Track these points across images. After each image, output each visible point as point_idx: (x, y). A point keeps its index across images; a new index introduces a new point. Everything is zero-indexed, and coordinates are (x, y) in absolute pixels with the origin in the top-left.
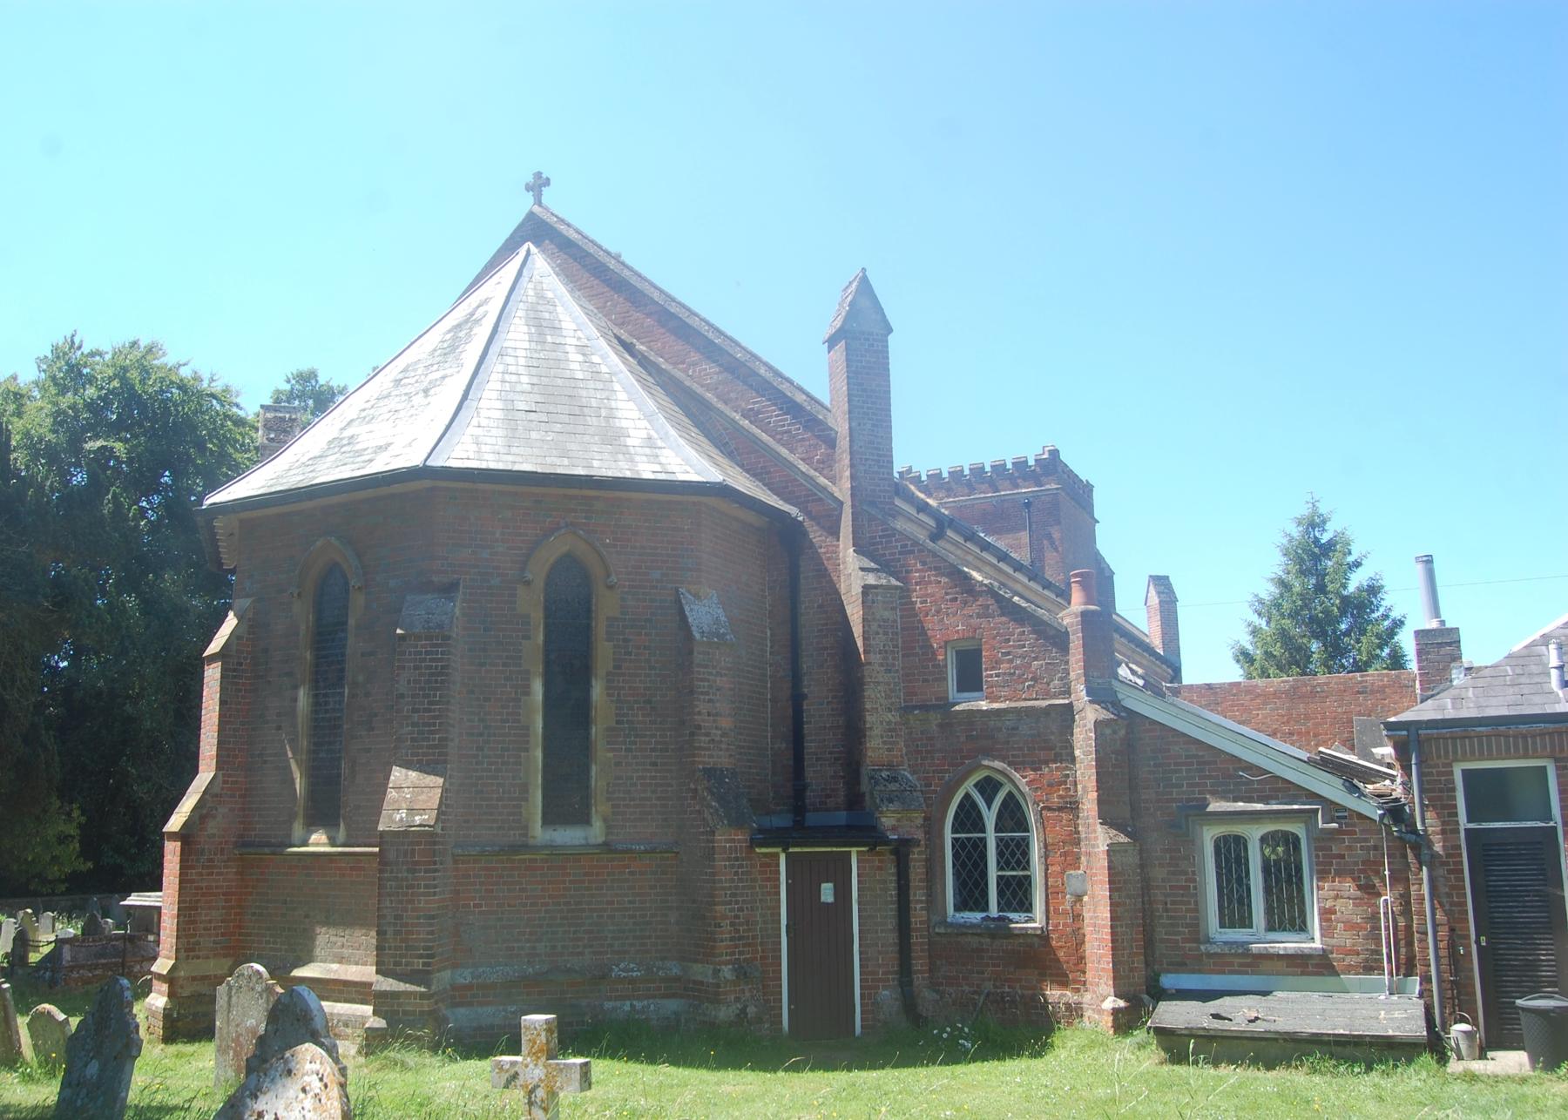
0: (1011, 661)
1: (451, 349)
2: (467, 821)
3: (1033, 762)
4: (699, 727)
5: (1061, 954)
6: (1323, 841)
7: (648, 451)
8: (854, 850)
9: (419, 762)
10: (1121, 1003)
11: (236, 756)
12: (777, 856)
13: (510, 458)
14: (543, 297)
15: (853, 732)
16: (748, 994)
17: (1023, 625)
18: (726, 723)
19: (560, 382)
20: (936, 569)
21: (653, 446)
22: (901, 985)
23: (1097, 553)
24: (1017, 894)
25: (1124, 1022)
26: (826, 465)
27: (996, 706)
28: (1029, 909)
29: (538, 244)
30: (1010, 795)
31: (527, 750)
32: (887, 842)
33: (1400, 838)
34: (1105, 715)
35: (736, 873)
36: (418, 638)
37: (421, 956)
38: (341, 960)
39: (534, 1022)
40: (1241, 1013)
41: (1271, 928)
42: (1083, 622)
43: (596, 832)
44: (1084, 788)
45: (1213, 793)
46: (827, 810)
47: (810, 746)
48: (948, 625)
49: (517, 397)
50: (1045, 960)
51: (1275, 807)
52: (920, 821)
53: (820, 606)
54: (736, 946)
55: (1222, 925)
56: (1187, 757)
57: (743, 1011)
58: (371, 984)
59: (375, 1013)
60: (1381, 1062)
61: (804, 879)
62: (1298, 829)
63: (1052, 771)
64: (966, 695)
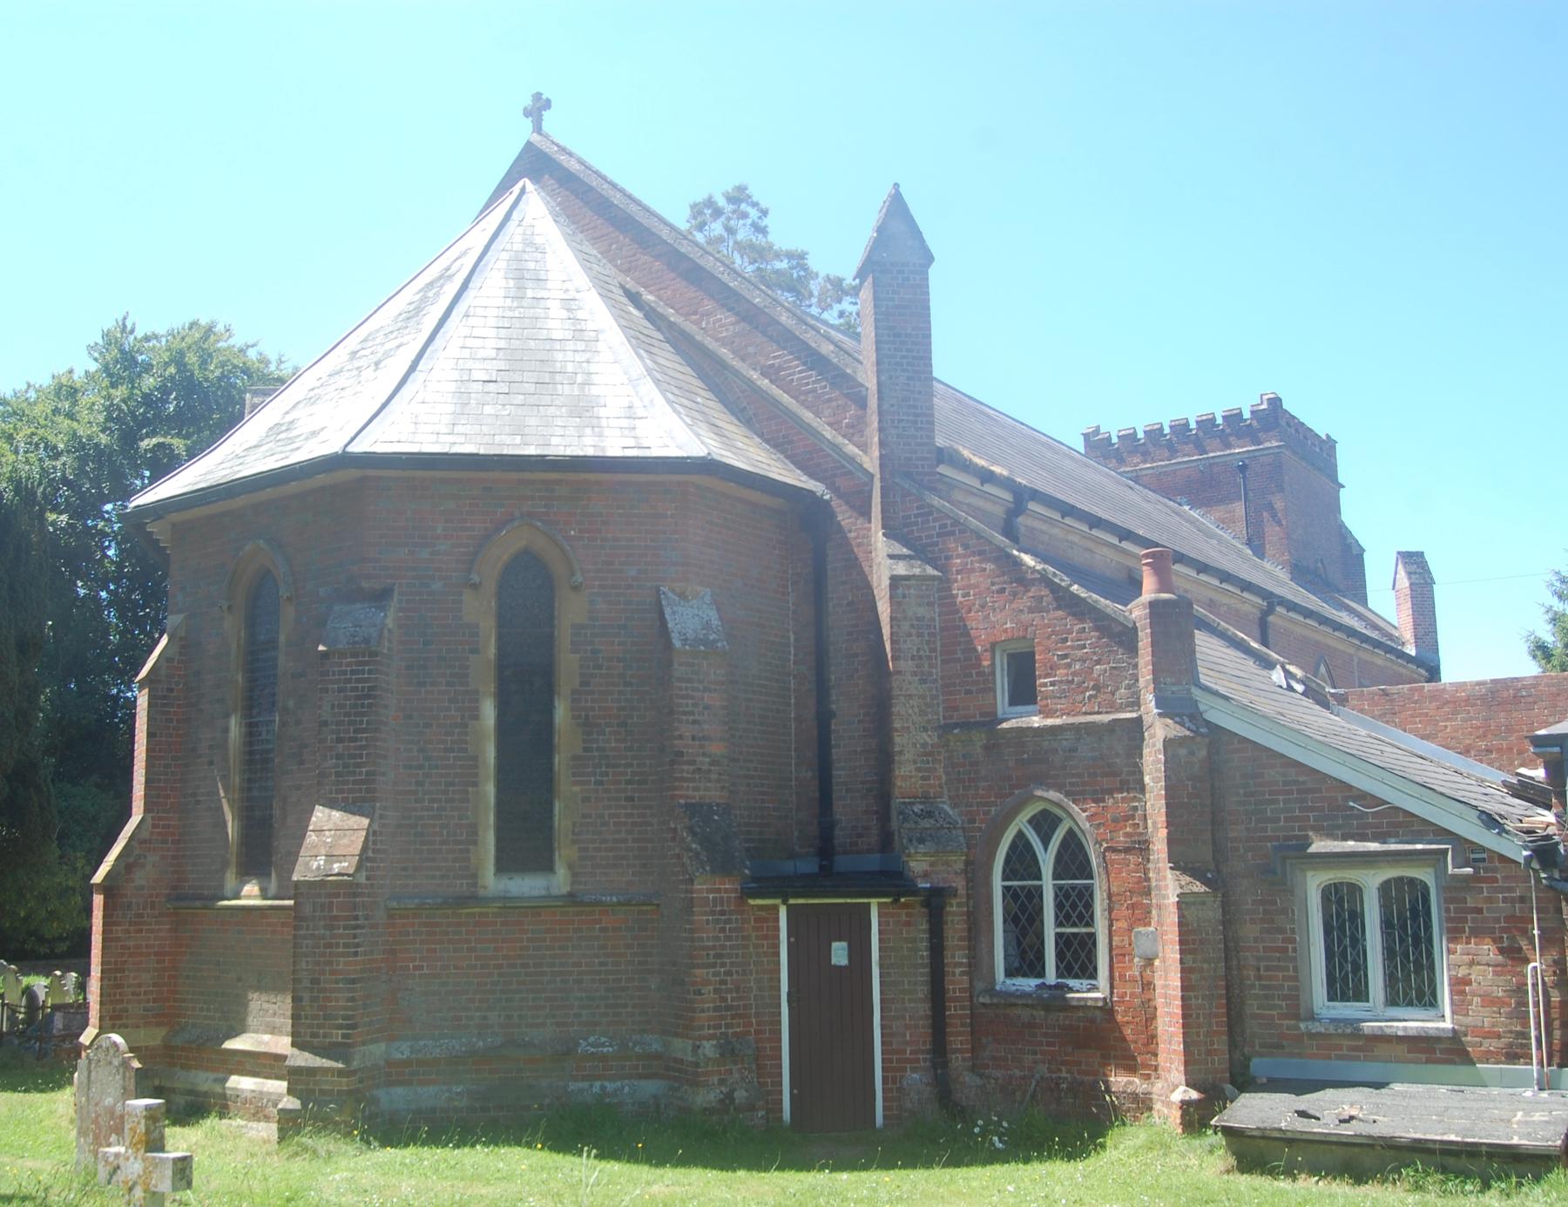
0: (1069, 666)
1: (416, 311)
2: (405, 869)
3: (1095, 792)
4: (680, 754)
5: (1128, 1031)
6: (1455, 889)
7: (625, 423)
8: (874, 902)
10: (1194, 1095)
11: (168, 797)
12: (775, 908)
13: (452, 438)
14: (532, 244)
15: (884, 758)
16: (736, 1076)
17: (1082, 621)
18: (717, 749)
19: (532, 344)
20: (981, 553)
21: (637, 412)
22: (935, 1066)
23: (1342, 526)
24: (1078, 957)
25: (1195, 1119)
26: (855, 430)
27: (1050, 722)
28: (1093, 975)
29: (536, 180)
30: (1070, 832)
31: (475, 784)
32: (913, 891)
33: (1550, 887)
34: (1177, 731)
35: (723, 930)
36: (342, 655)
37: (340, 1027)
39: (135, 1108)
40: (1340, 1110)
41: (1392, 1001)
42: (1152, 615)
43: (560, 882)
44: (1154, 823)
45: (1314, 828)
46: (858, 852)
47: (839, 774)
48: (994, 621)
49: (478, 365)
50: (1106, 1039)
51: (1393, 847)
52: (960, 866)
53: (850, 604)
54: (722, 1018)
55: (1332, 997)
56: (1285, 783)
57: (730, 1096)
58: (284, 1057)
59: (290, 1091)
60: (1500, 1179)
61: (810, 937)
62: (1425, 875)
63: (1117, 802)
64: (1020, 709)
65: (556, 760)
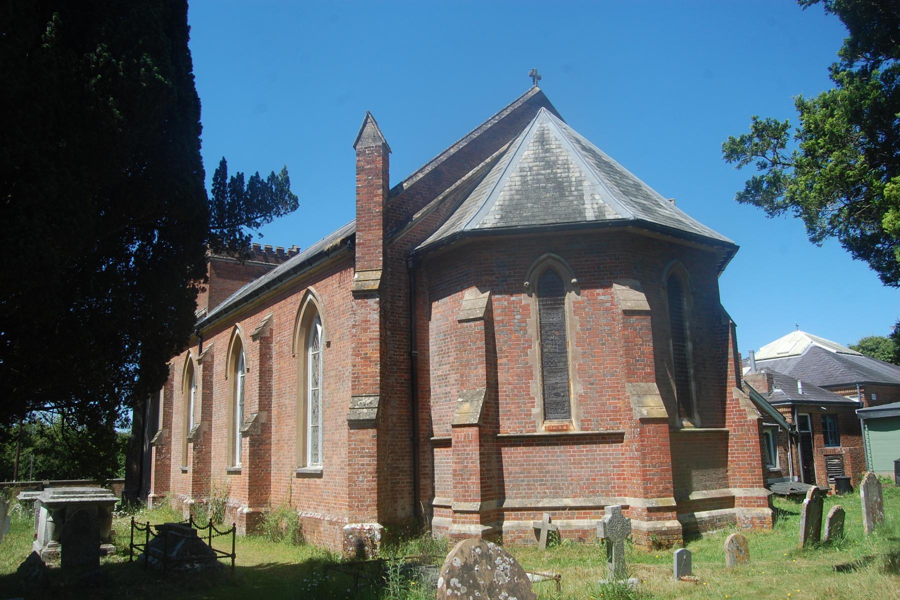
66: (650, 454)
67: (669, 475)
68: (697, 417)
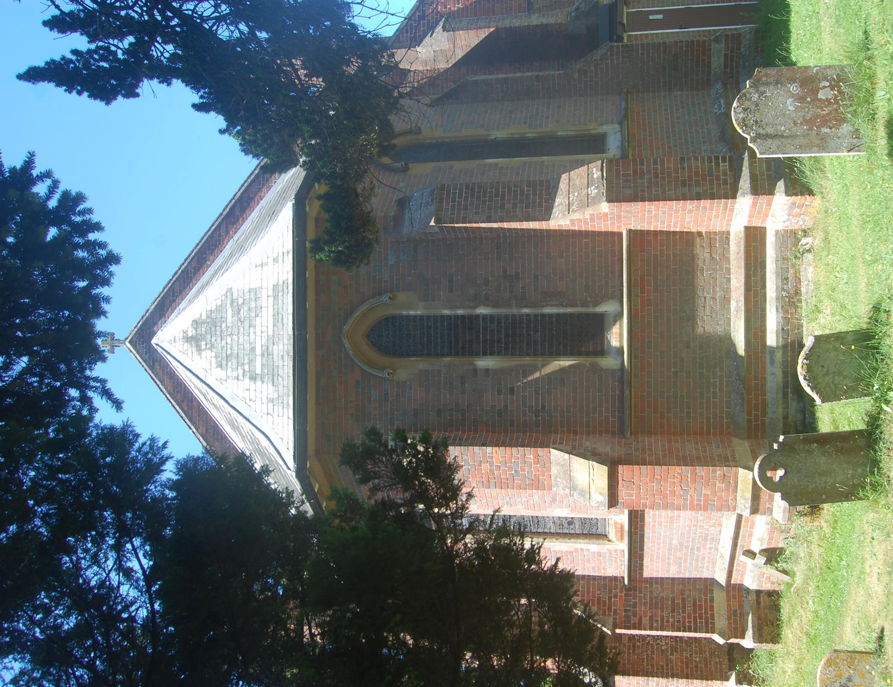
9: (547, 201)
12: (629, 36)
37: (717, 164)
38: (727, 300)
65: (530, 135)
66: (665, 496)
67: (701, 471)
68: (607, 308)
